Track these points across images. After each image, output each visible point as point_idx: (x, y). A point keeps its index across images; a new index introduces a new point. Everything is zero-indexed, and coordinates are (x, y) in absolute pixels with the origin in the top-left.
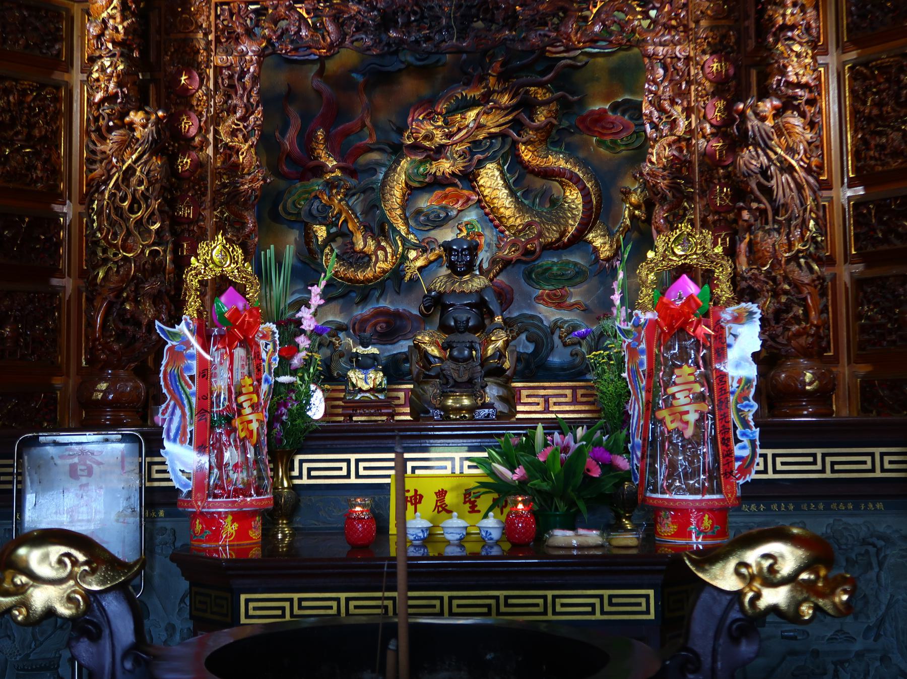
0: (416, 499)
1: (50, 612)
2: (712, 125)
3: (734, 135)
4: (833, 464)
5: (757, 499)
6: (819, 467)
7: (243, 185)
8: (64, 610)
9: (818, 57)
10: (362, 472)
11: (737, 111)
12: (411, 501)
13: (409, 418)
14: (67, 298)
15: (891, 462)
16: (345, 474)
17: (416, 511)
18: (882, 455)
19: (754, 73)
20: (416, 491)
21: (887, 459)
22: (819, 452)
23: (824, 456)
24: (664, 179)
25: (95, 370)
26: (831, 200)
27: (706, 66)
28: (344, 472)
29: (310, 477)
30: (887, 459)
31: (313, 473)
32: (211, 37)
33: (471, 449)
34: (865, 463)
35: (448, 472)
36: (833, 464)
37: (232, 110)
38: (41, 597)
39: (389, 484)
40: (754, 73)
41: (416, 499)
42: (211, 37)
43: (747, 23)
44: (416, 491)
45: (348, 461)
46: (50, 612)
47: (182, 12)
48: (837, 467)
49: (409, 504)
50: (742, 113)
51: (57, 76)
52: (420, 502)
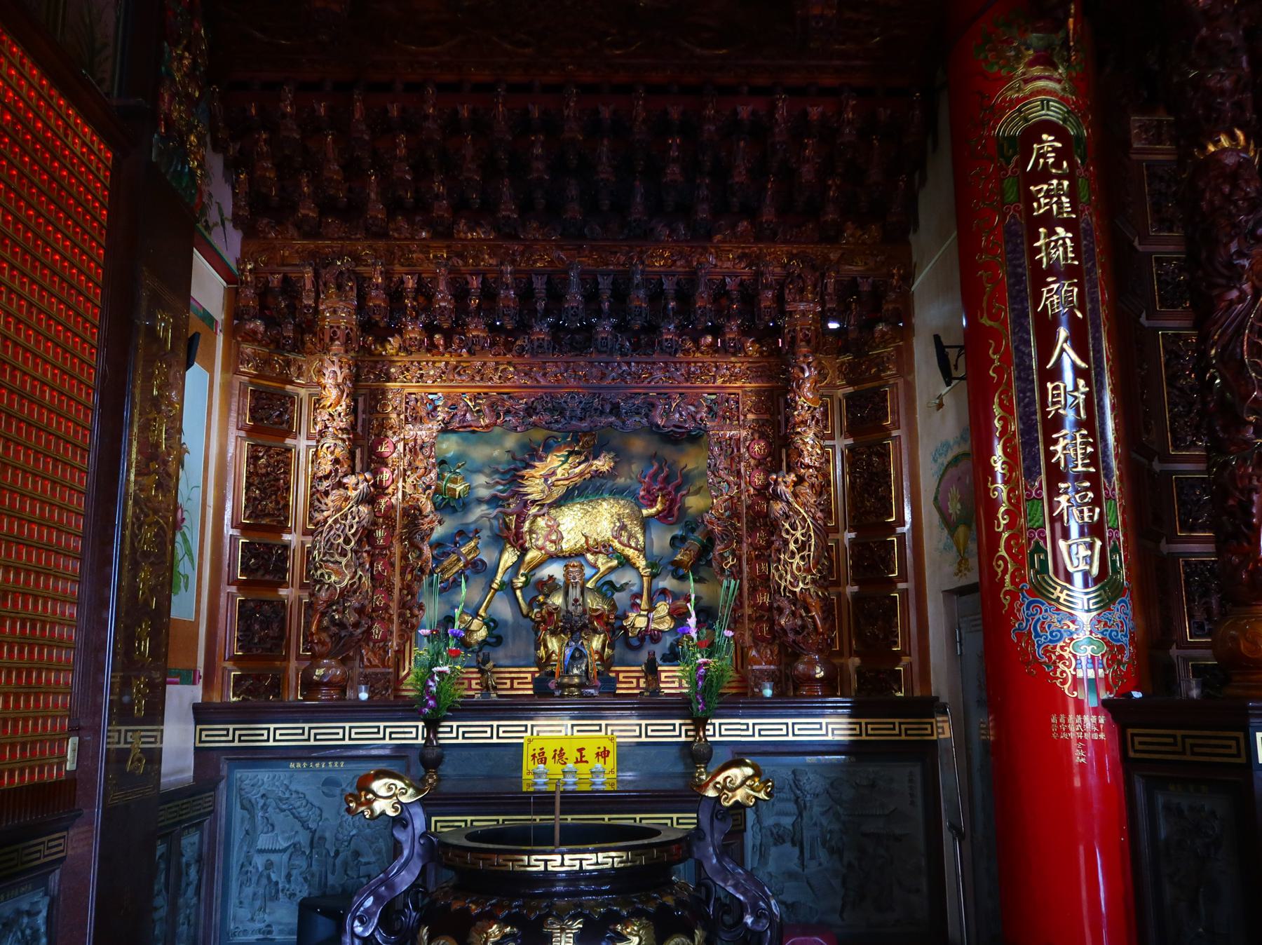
1: (383, 813)
3: (767, 493)
5: (395, 845)
8: (391, 813)
13: (531, 692)
18: (343, 739)
19: (784, 451)
21: (870, 727)
23: (900, 724)
25: (315, 659)
28: (341, 736)
29: (240, 741)
30: (870, 727)
32: (402, 417)
35: (563, 734)
38: (379, 806)
40: (784, 451)
42: (402, 417)
45: (492, 726)
46: (383, 813)
50: (776, 481)
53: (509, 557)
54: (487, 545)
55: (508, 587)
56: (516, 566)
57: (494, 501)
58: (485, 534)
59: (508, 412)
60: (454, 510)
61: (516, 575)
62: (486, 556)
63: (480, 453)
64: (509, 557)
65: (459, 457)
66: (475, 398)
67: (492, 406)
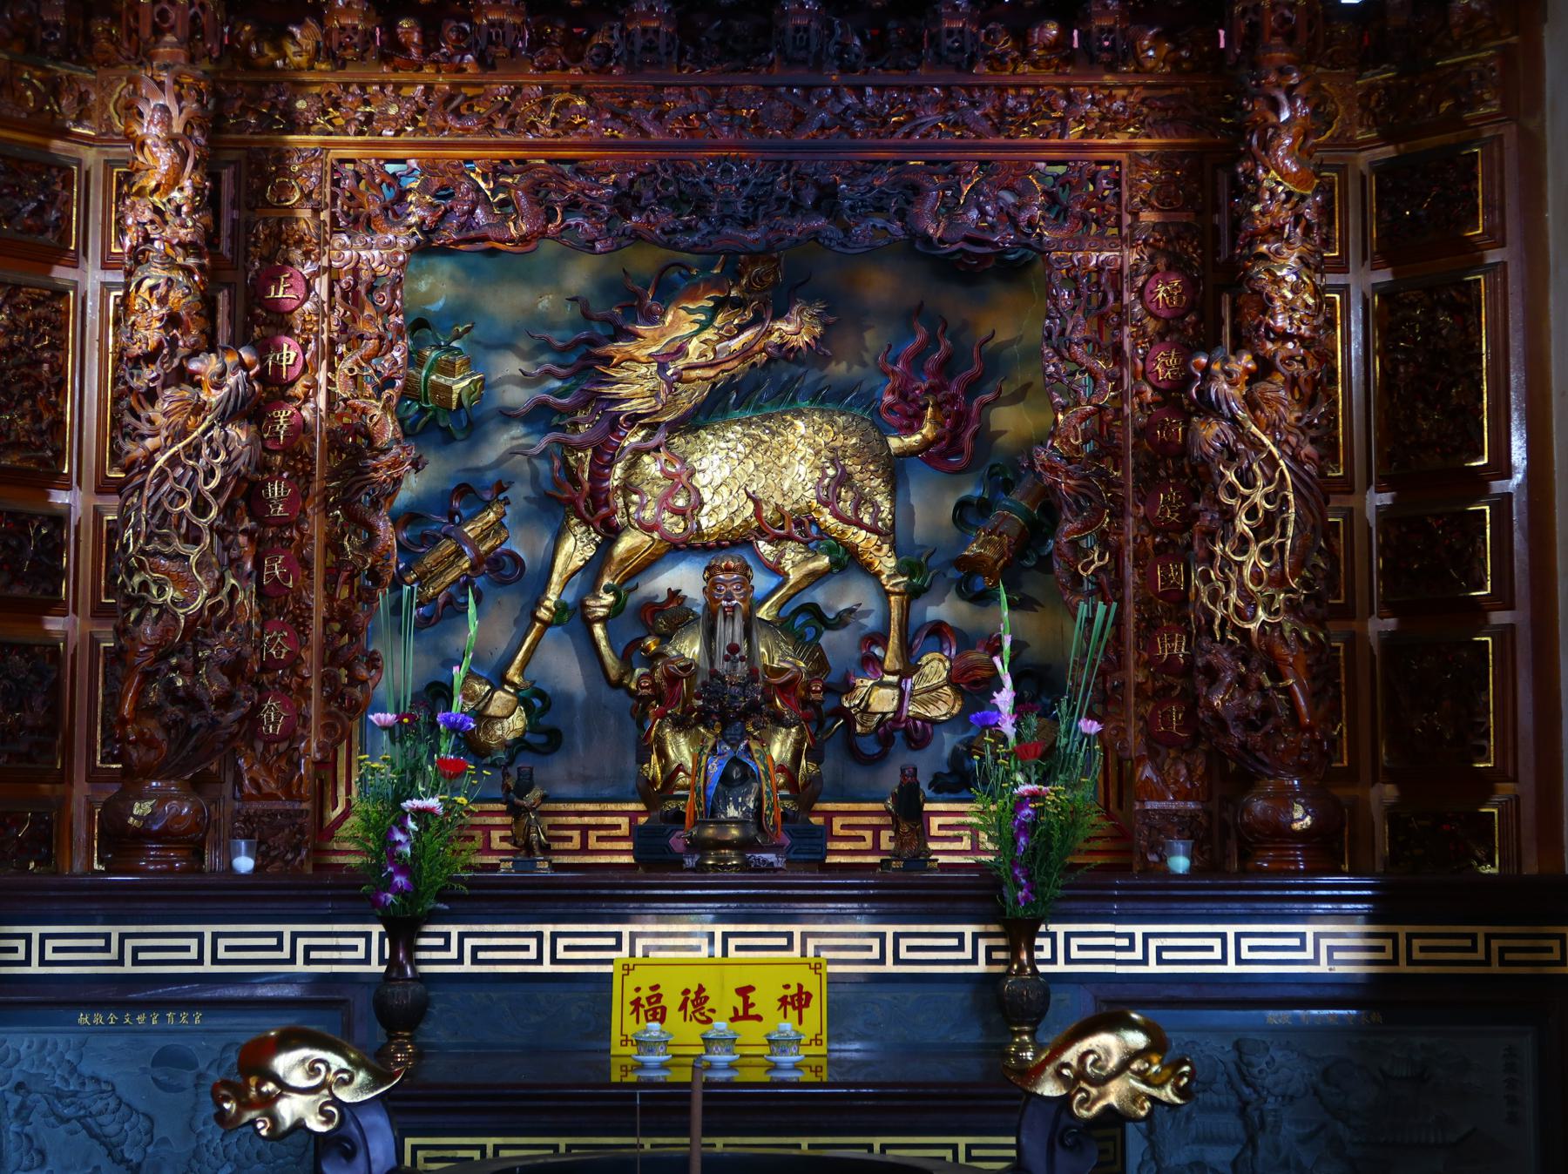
0: (800, 1000)
2: (1154, 388)
3: (1184, 400)
4: (475, 949)
6: (1480, 955)
7: (376, 470)
9: (232, 168)
10: (1075, 954)
11: (1197, 365)
12: (792, 1004)
14: (70, 652)
15: (1550, 950)
16: (1219, 956)
17: (800, 1022)
19: (1226, 298)
20: (800, 987)
22: (1481, 931)
24: (1069, 477)
25: (132, 780)
26: (1349, 515)
27: (1147, 291)
31: (1166, 955)
33: (721, 918)
34: (910, 949)
36: (475, 949)
37: (357, 339)
39: (611, 974)
40: (1226, 298)
41: (800, 1000)
43: (1217, 219)
44: (800, 987)
47: (277, 174)
48: (1508, 956)
49: (789, 1008)
50: (1206, 370)
51: (61, 273)
52: (807, 1005)
53: (575, 550)
54: (524, 519)
55: (574, 617)
56: (593, 569)
57: (539, 416)
58: (520, 492)
59: (572, 206)
60: (448, 438)
61: (593, 588)
62: (523, 544)
63: (507, 303)
64: (575, 550)
65: (459, 313)
66: (495, 171)
67: (536, 190)
